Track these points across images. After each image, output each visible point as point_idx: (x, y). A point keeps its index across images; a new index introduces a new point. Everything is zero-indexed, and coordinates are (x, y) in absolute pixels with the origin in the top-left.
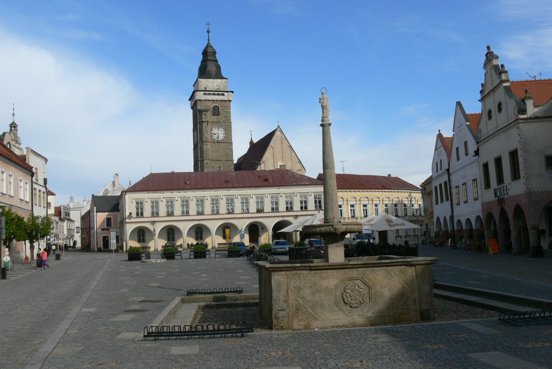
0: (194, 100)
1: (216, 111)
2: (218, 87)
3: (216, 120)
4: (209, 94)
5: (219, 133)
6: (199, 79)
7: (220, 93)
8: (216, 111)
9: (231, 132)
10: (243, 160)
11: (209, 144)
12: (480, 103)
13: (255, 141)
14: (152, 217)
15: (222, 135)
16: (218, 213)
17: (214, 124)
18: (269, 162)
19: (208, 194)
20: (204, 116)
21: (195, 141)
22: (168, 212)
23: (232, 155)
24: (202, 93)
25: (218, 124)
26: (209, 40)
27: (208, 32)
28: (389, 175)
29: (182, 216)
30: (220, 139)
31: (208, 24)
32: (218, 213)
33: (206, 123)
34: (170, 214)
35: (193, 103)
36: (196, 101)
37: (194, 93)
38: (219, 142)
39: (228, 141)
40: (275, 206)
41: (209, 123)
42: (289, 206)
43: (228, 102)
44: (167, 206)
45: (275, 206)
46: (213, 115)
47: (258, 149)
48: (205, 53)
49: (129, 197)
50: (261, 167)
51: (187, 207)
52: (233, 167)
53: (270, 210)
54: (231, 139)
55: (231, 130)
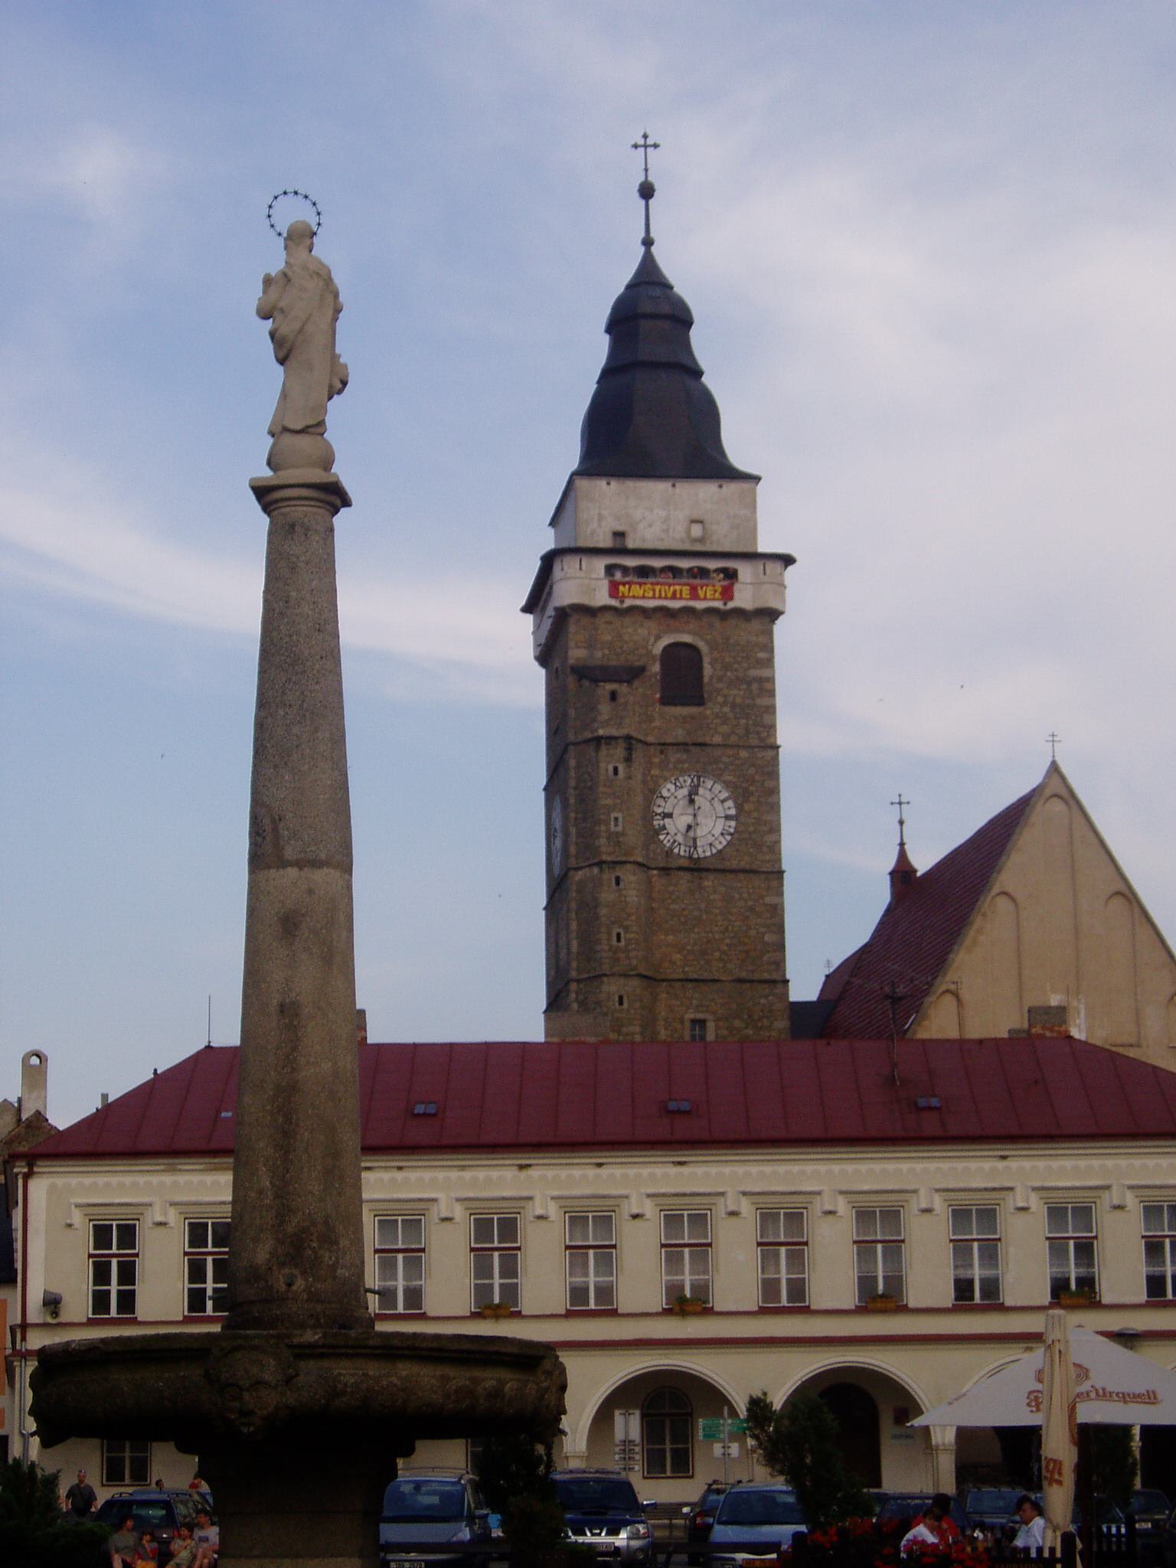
0: (550, 611)
1: (682, 679)
2: (696, 531)
3: (679, 734)
4: (644, 572)
5: (698, 818)
6: (582, 484)
7: (658, 563)
8: (682, 679)
9: (775, 808)
10: (848, 979)
11: (631, 877)
12: (529, 619)
13: (923, 862)
14: (955, 1310)
15: (720, 826)
16: (800, 1307)
17: (674, 756)
18: (978, 999)
19: (638, 1183)
20: (605, 709)
21: (557, 861)
22: (866, 1283)
23: (781, 947)
24: (600, 564)
25: (695, 755)
26: (648, 242)
27: (647, 191)
28: (105, 1097)
29: (569, 1314)
30: (703, 851)
31: (646, 144)
32: (800, 1307)
33: (620, 751)
34: (881, 1297)
35: (547, 624)
36: (563, 615)
37: (549, 561)
38: (697, 868)
39: (753, 867)
40: (1073, 1273)
41: (638, 755)
42: (977, 1273)
43: (756, 625)
44: (672, 1251)
45: (1073, 1273)
46: (665, 701)
47: (933, 906)
48: (626, 321)
49: (52, 1190)
50: (939, 1022)
51: (797, 1259)
52: (782, 1024)
53: (946, 1296)
54: (775, 849)
55: (775, 791)
